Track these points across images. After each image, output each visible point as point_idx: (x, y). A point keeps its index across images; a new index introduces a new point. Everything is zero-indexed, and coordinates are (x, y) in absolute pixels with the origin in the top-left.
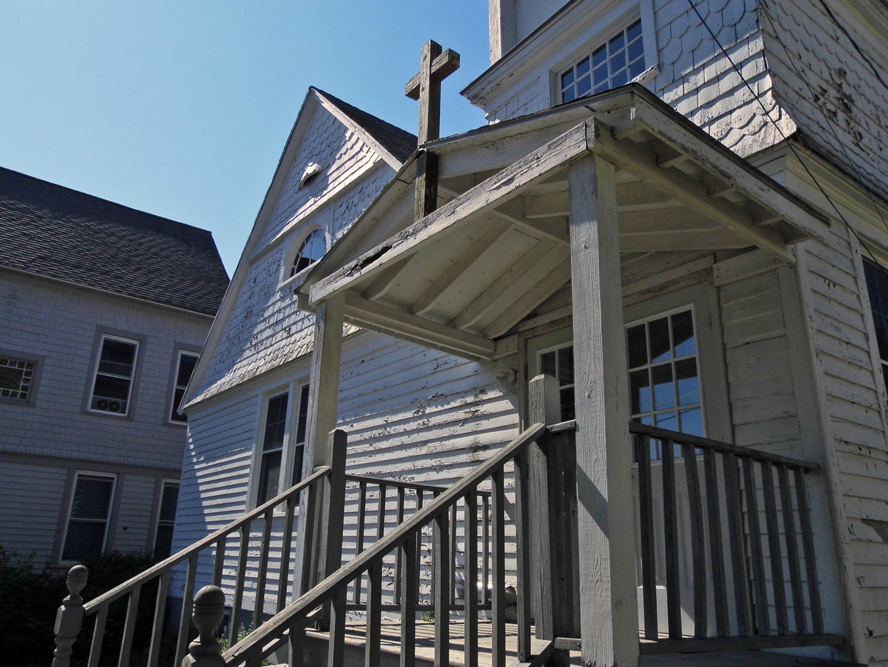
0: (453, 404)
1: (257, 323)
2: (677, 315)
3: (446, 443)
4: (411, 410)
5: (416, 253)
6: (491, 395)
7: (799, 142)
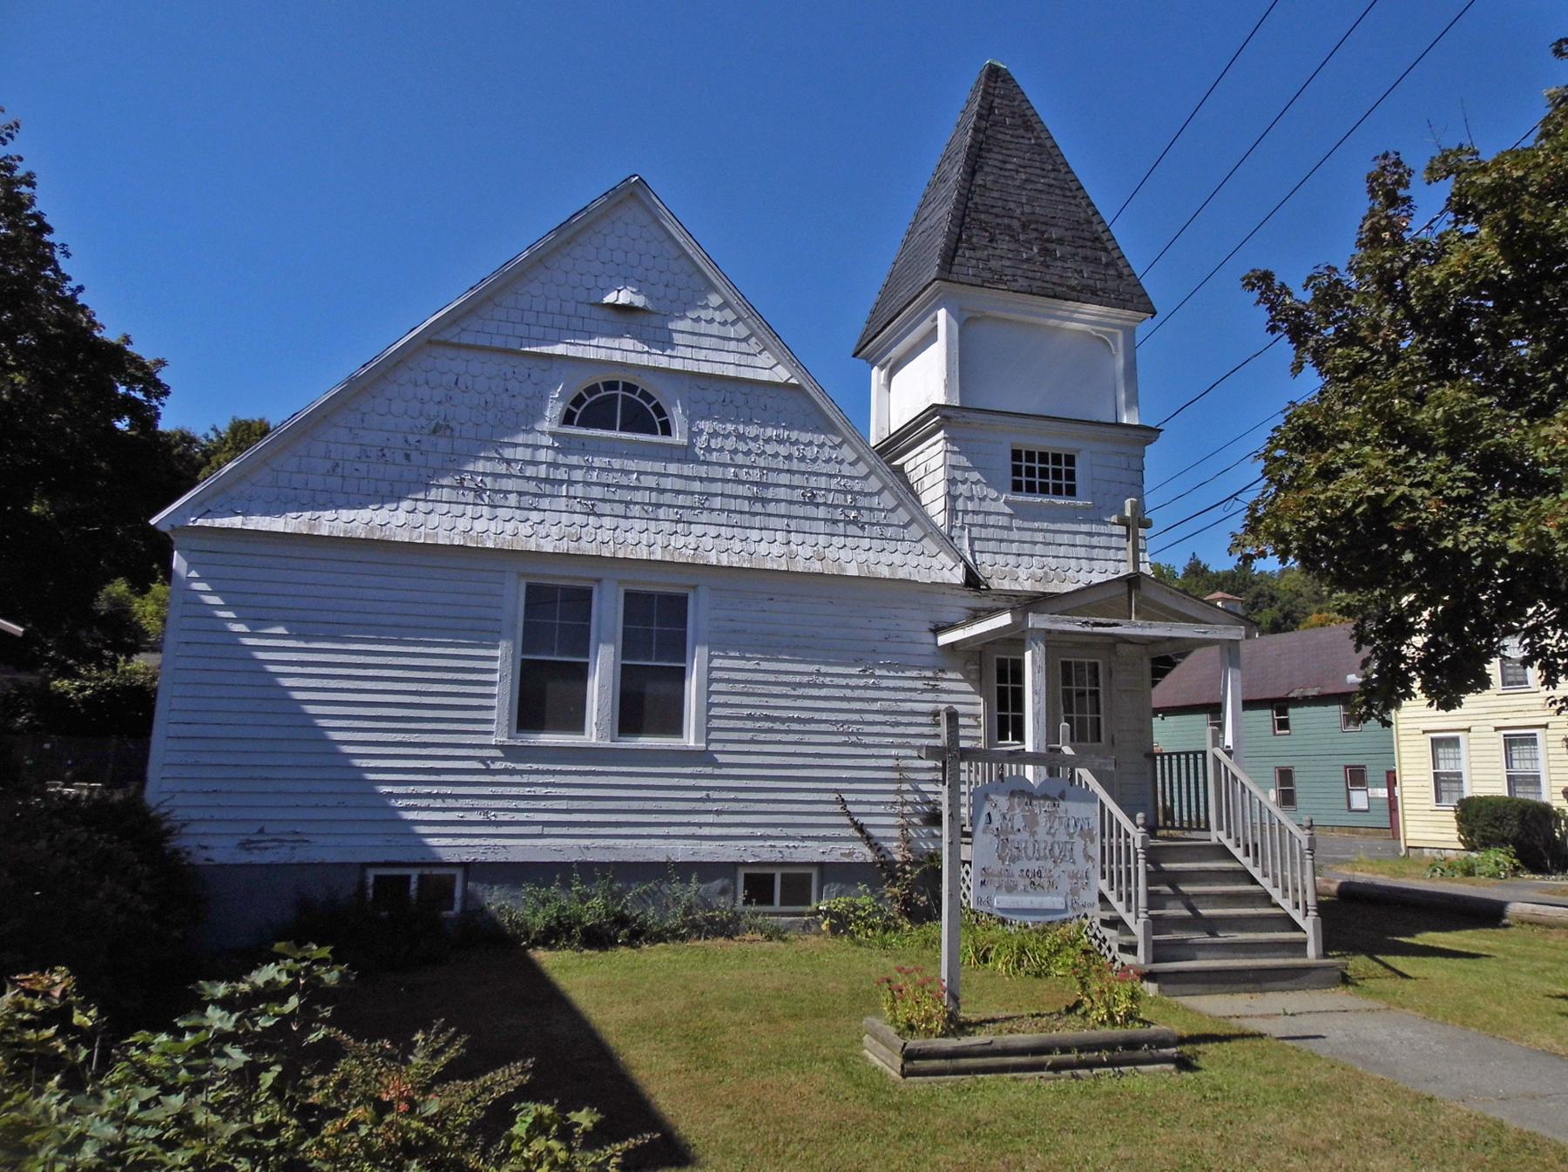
0: (908, 674)
1: (477, 458)
2: (589, 631)
3: (902, 704)
4: (858, 667)
5: (1411, 978)
6: (950, 675)
7: (20, 1161)
